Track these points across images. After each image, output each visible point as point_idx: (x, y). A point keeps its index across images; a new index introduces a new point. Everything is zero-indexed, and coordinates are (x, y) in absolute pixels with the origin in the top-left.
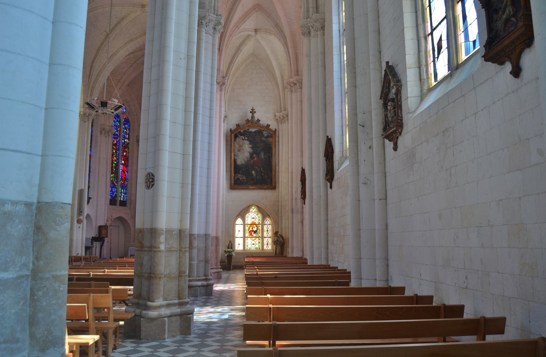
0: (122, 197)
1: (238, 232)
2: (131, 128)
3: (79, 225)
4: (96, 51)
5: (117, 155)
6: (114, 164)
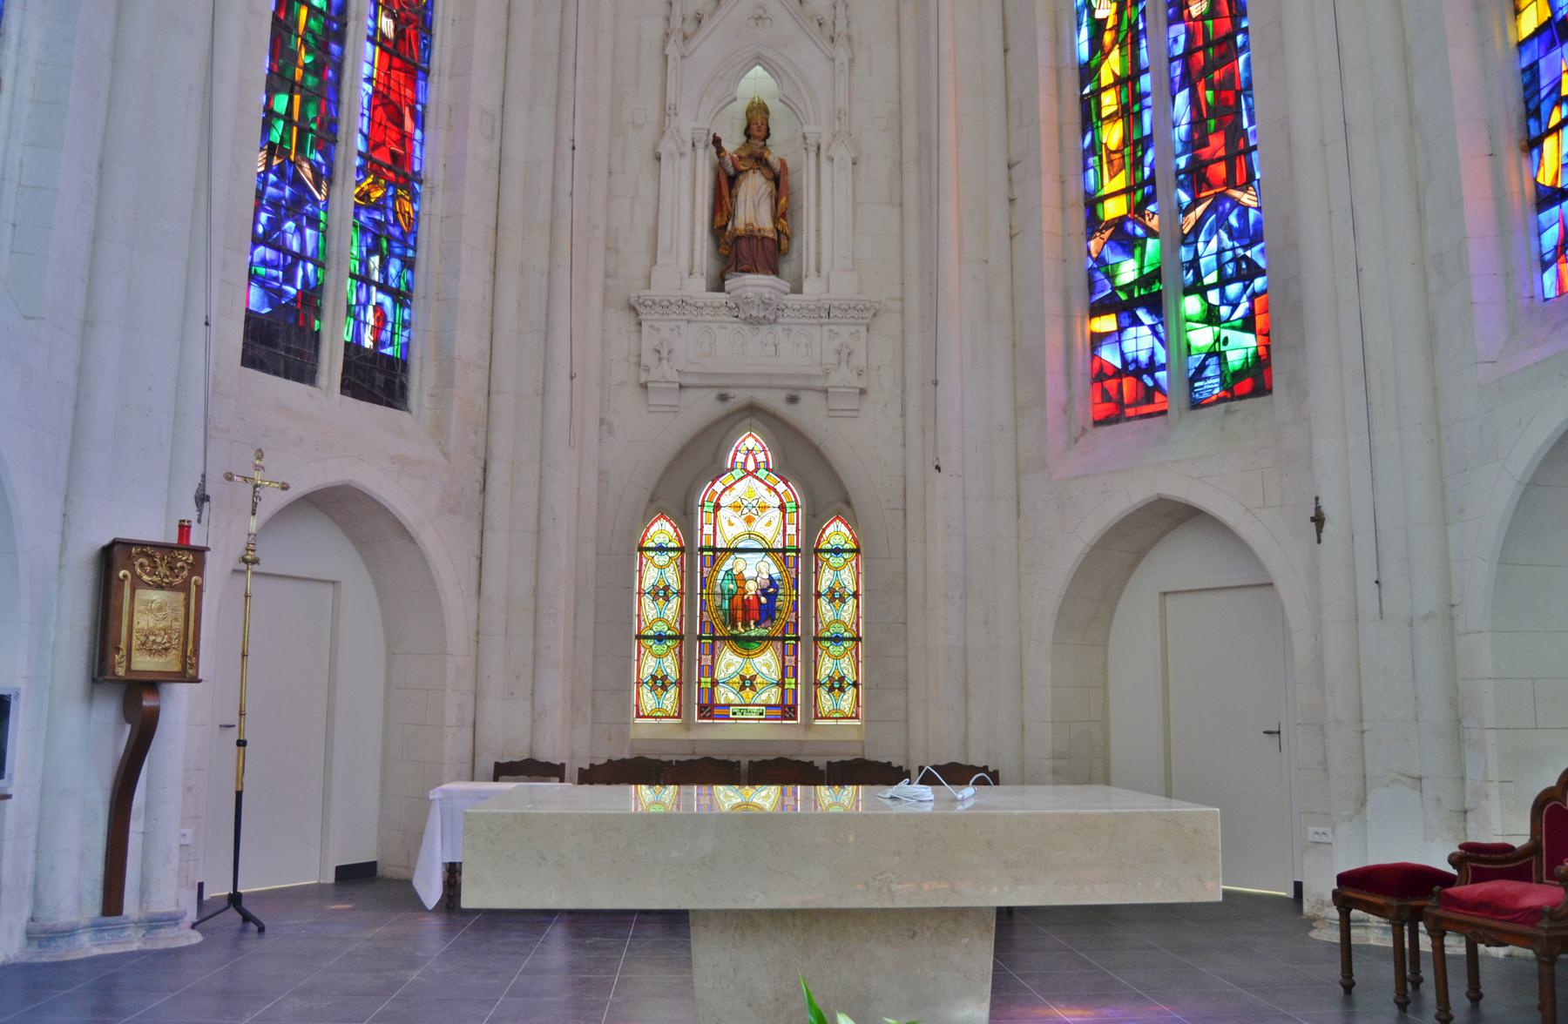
0: (370, 317)
6: (304, 12)
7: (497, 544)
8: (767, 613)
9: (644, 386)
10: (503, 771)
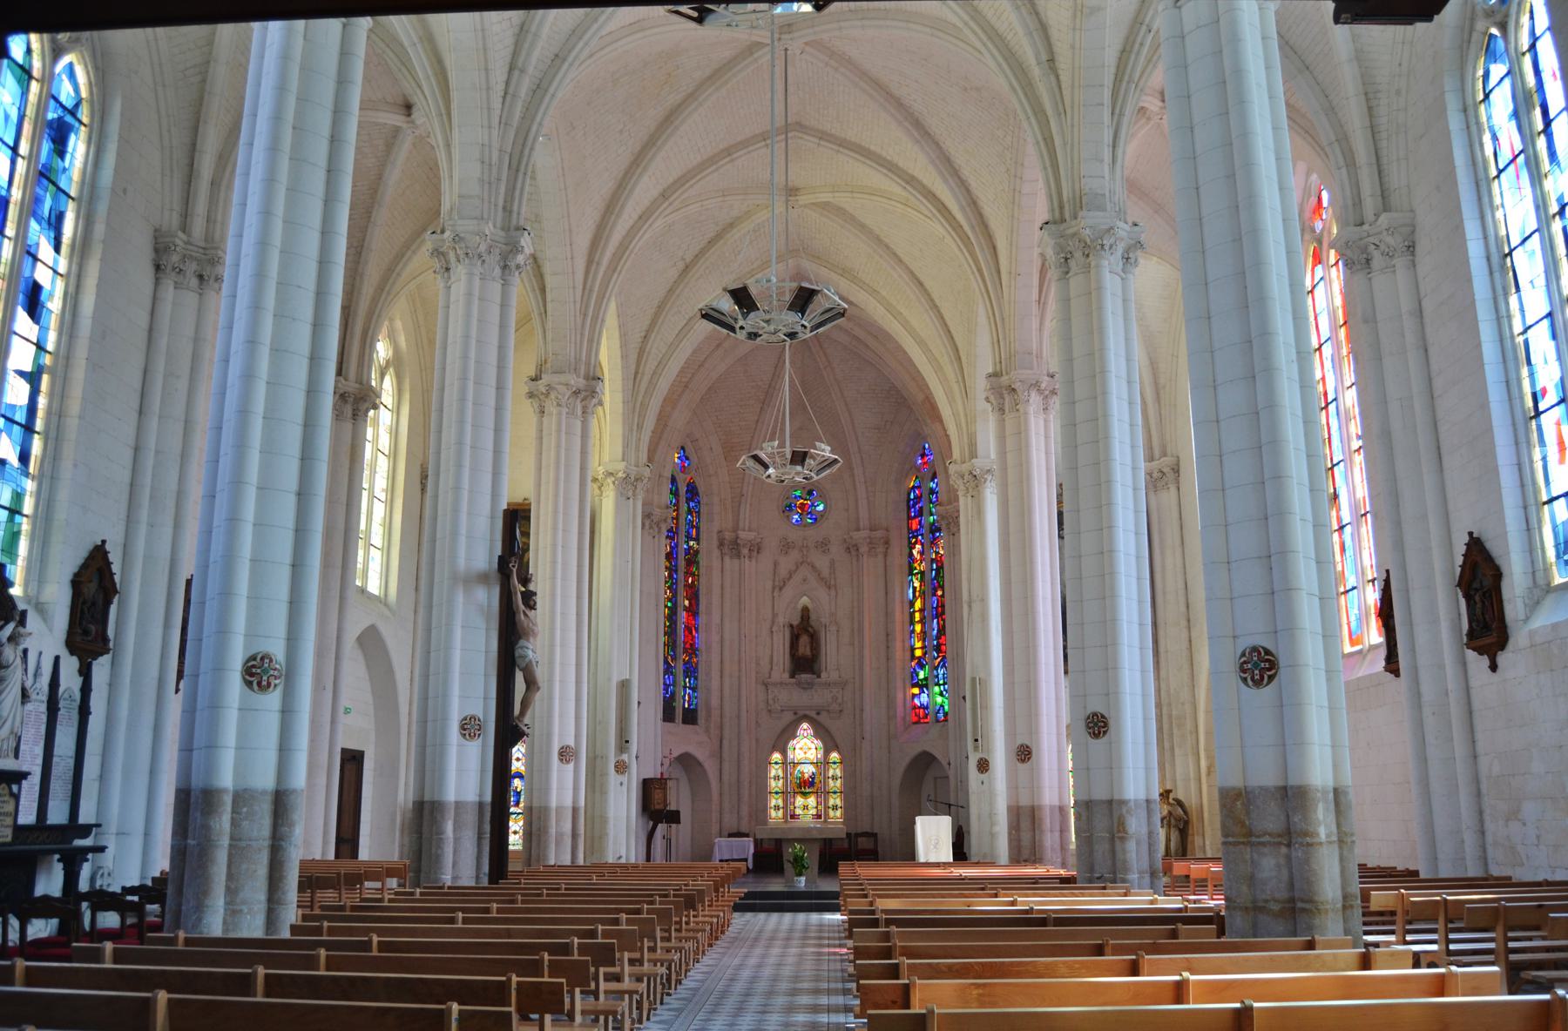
0: (687, 698)
2: (704, 509)
3: (983, 776)
4: (653, 310)
5: (672, 583)
7: (726, 766)
8: (812, 784)
9: (770, 711)
10: (730, 835)
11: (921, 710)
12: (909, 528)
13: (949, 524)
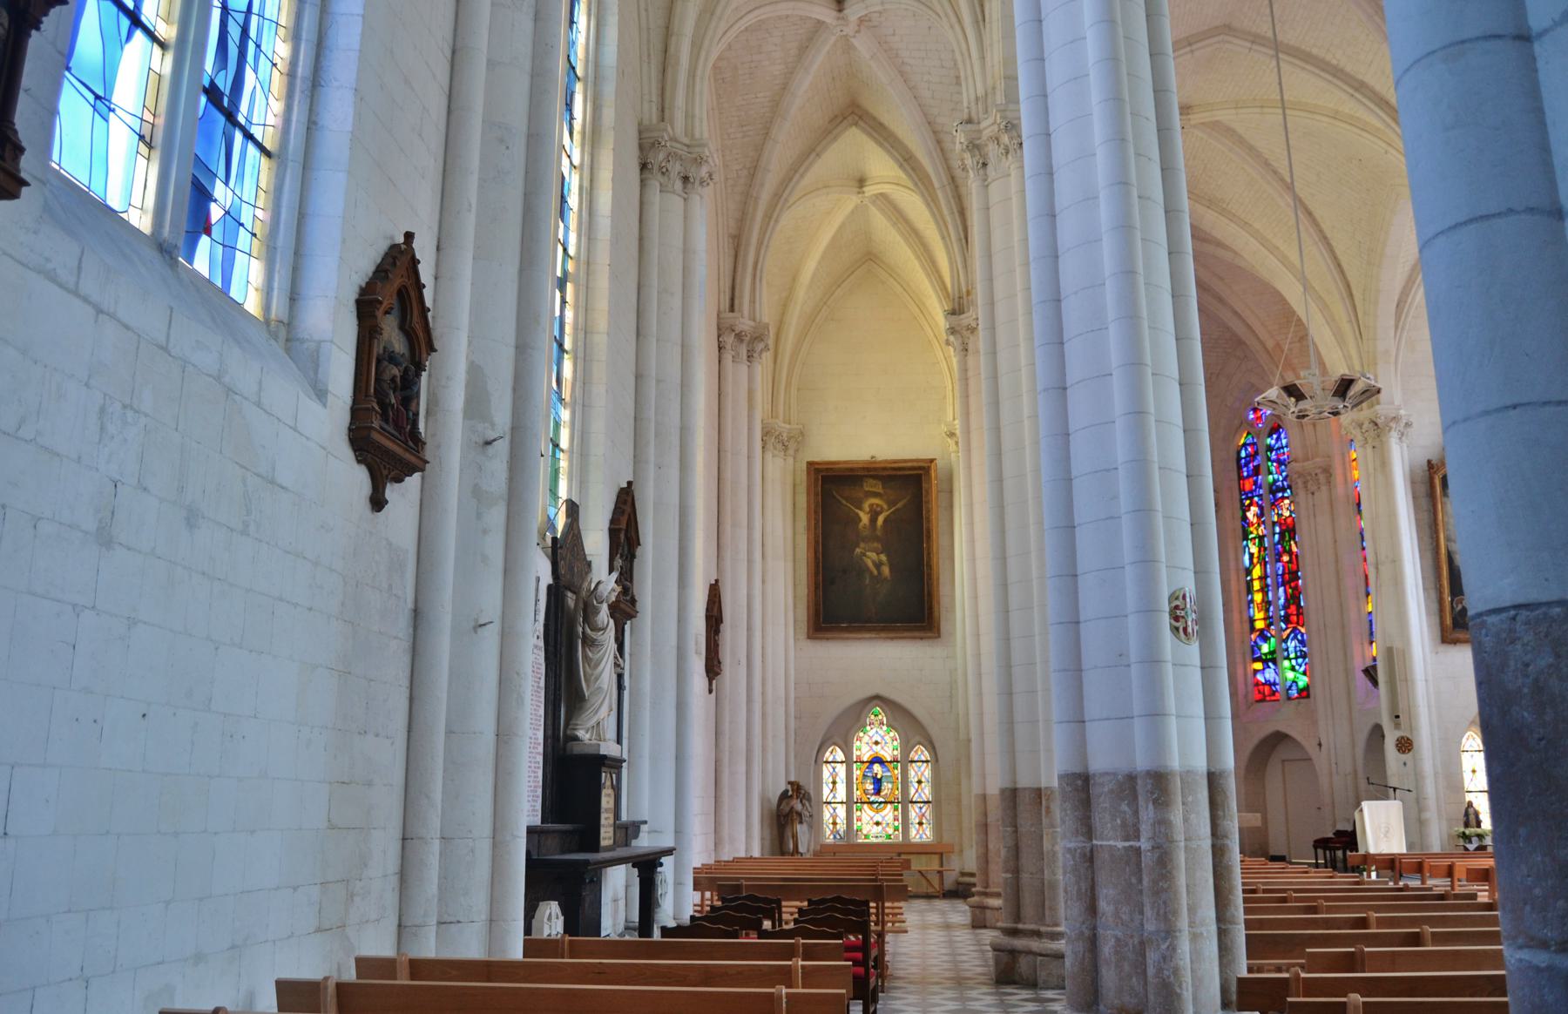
1: (1471, 774)
3: (1404, 757)
11: (1267, 688)
12: (1241, 490)
13: (1305, 483)
